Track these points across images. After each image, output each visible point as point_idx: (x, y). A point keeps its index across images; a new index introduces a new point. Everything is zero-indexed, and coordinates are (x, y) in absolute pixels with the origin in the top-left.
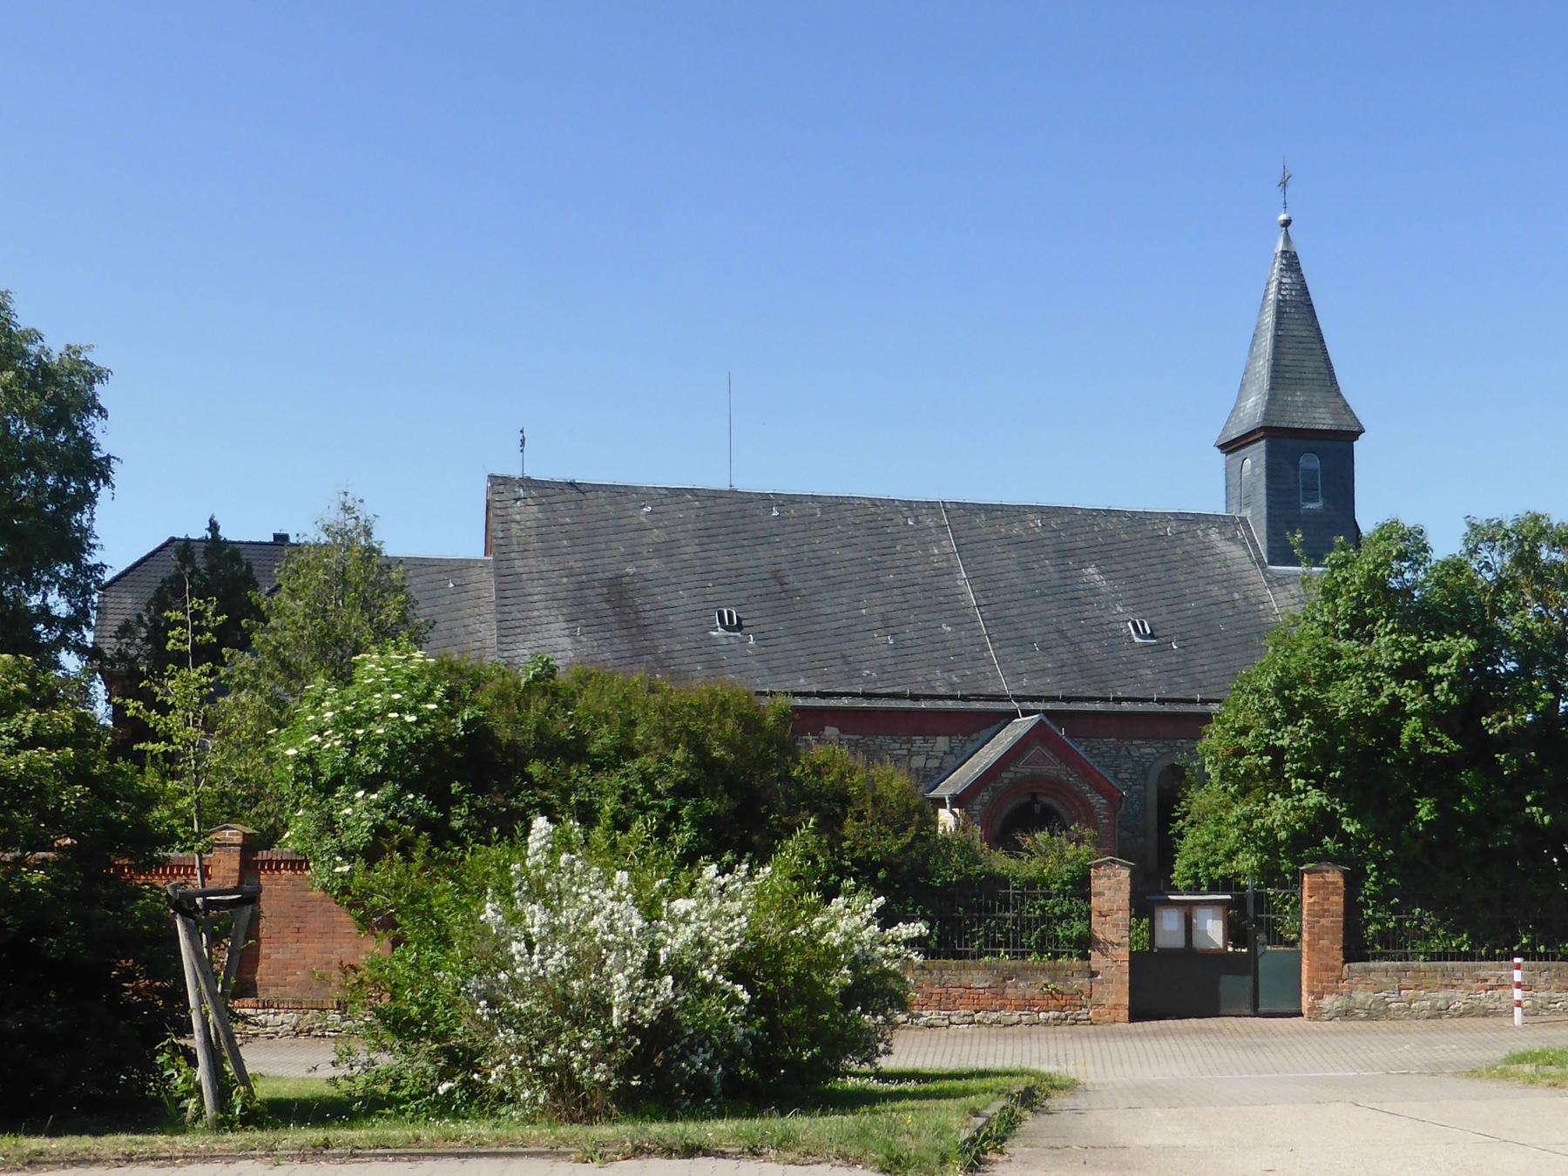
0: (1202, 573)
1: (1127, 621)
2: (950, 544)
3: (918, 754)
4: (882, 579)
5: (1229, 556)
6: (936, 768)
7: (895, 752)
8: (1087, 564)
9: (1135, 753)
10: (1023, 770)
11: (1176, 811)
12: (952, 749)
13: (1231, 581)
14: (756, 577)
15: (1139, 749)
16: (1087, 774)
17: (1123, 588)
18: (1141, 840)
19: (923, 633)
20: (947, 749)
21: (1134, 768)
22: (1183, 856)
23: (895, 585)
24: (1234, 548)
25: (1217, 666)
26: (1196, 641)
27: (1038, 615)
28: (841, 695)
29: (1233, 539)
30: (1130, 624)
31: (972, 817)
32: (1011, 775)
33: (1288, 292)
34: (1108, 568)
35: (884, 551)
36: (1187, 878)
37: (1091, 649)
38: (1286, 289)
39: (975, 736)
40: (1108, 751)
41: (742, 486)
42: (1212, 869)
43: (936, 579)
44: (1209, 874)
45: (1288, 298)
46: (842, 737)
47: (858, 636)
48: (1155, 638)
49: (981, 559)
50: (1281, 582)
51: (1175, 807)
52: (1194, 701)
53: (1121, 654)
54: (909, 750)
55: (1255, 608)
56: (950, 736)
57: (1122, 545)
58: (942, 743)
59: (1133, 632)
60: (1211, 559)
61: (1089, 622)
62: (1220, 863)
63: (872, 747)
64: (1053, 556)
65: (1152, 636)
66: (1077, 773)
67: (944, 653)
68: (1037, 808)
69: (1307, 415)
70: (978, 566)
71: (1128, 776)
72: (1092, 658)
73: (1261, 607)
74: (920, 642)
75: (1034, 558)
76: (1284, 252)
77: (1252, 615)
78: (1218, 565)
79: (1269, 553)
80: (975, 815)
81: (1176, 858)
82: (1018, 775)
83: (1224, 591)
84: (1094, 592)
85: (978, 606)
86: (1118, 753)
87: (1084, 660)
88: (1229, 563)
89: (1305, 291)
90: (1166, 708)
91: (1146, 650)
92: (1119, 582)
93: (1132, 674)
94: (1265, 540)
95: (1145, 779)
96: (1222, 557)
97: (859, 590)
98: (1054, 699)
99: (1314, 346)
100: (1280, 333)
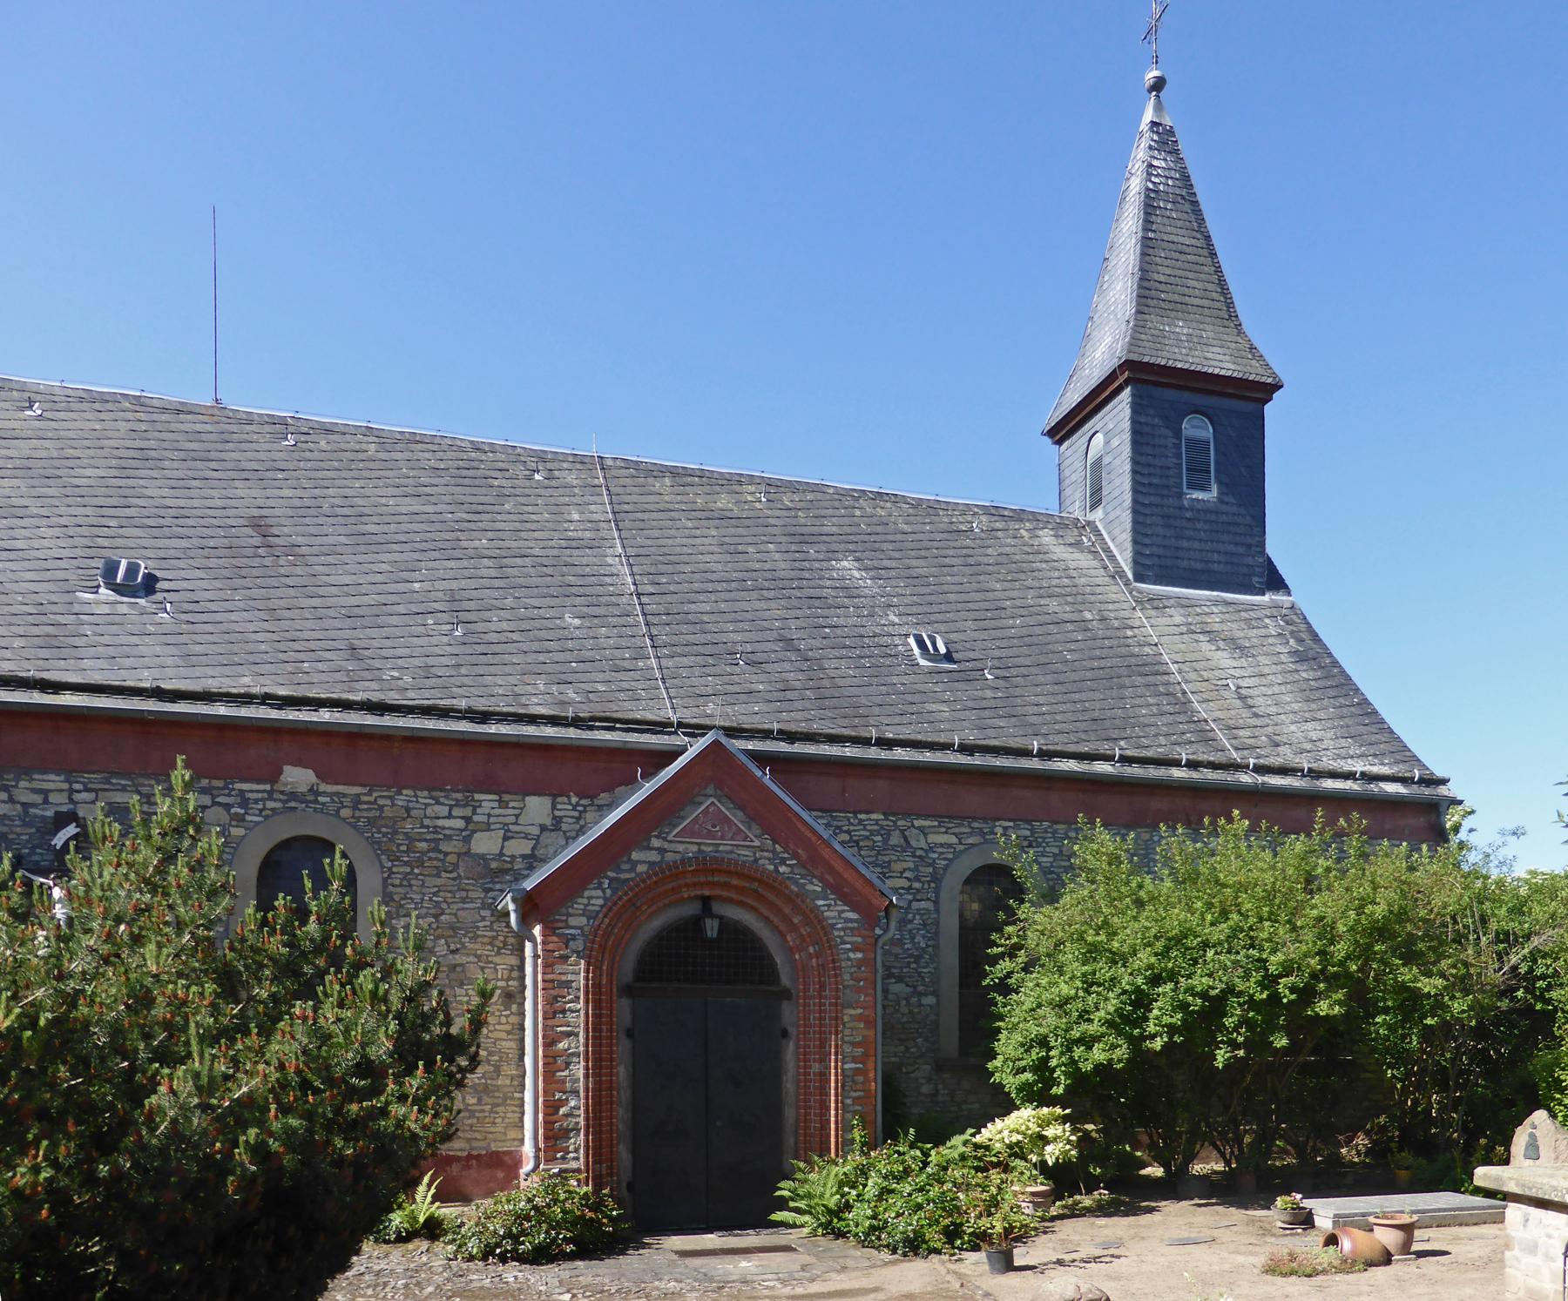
0: (1030, 583)
1: (907, 636)
2: (602, 509)
3: (487, 827)
4: (465, 544)
5: (1072, 565)
6: (524, 857)
7: (440, 822)
8: (840, 556)
9: (918, 842)
10: (681, 848)
11: (994, 944)
12: (557, 821)
13: (1077, 596)
14: (216, 522)
15: (925, 835)
16: (815, 858)
17: (900, 591)
18: (929, 1000)
19: (525, 625)
20: (548, 822)
21: (916, 869)
22: (1015, 1026)
23: (487, 553)
24: (1077, 555)
25: (1062, 708)
26: (1023, 671)
27: (749, 616)
28: (318, 704)
29: (1077, 545)
30: (911, 641)
31: (567, 940)
32: (653, 856)
33: (1163, 180)
34: (876, 563)
35: (481, 508)
36: (1024, 1070)
37: (840, 668)
38: (1158, 175)
39: (604, 798)
40: (867, 838)
41: (238, 403)
42: (1078, 1052)
43: (568, 552)
44: (1073, 1062)
45: (1161, 188)
46: (323, 787)
47: (394, 620)
48: (955, 662)
49: (656, 533)
50: (1156, 603)
51: (994, 936)
52: (1025, 753)
53: (895, 680)
54: (468, 820)
55: (1118, 634)
56: (554, 796)
57: (899, 537)
58: (537, 808)
59: (916, 651)
60: (1044, 565)
61: (839, 632)
62: (1096, 1039)
63: (388, 812)
64: (783, 539)
65: (948, 657)
66: (795, 856)
67: (560, 657)
68: (711, 928)
69: (1193, 353)
70: (649, 542)
71: (906, 884)
72: (840, 682)
73: (1129, 633)
74: (515, 636)
75: (749, 540)
76: (1153, 123)
77: (1114, 642)
78: (1056, 574)
79: (1136, 563)
80: (574, 938)
81: (998, 1031)
82: (669, 857)
83: (1068, 609)
84: (850, 591)
85: (639, 595)
86: (886, 841)
87: (826, 683)
88: (1074, 574)
89: (1186, 178)
90: (977, 760)
91: (937, 678)
92: (894, 582)
93: (914, 708)
94: (1128, 546)
95: (937, 891)
96: (1062, 565)
97: (416, 556)
98: (766, 734)
99: (1201, 260)
100: (1151, 235)
